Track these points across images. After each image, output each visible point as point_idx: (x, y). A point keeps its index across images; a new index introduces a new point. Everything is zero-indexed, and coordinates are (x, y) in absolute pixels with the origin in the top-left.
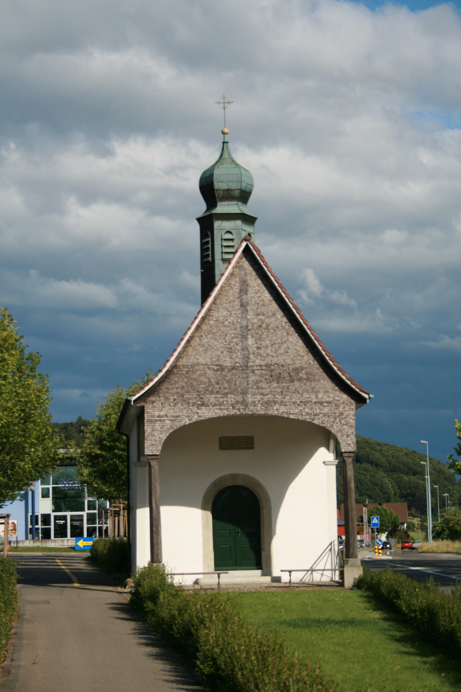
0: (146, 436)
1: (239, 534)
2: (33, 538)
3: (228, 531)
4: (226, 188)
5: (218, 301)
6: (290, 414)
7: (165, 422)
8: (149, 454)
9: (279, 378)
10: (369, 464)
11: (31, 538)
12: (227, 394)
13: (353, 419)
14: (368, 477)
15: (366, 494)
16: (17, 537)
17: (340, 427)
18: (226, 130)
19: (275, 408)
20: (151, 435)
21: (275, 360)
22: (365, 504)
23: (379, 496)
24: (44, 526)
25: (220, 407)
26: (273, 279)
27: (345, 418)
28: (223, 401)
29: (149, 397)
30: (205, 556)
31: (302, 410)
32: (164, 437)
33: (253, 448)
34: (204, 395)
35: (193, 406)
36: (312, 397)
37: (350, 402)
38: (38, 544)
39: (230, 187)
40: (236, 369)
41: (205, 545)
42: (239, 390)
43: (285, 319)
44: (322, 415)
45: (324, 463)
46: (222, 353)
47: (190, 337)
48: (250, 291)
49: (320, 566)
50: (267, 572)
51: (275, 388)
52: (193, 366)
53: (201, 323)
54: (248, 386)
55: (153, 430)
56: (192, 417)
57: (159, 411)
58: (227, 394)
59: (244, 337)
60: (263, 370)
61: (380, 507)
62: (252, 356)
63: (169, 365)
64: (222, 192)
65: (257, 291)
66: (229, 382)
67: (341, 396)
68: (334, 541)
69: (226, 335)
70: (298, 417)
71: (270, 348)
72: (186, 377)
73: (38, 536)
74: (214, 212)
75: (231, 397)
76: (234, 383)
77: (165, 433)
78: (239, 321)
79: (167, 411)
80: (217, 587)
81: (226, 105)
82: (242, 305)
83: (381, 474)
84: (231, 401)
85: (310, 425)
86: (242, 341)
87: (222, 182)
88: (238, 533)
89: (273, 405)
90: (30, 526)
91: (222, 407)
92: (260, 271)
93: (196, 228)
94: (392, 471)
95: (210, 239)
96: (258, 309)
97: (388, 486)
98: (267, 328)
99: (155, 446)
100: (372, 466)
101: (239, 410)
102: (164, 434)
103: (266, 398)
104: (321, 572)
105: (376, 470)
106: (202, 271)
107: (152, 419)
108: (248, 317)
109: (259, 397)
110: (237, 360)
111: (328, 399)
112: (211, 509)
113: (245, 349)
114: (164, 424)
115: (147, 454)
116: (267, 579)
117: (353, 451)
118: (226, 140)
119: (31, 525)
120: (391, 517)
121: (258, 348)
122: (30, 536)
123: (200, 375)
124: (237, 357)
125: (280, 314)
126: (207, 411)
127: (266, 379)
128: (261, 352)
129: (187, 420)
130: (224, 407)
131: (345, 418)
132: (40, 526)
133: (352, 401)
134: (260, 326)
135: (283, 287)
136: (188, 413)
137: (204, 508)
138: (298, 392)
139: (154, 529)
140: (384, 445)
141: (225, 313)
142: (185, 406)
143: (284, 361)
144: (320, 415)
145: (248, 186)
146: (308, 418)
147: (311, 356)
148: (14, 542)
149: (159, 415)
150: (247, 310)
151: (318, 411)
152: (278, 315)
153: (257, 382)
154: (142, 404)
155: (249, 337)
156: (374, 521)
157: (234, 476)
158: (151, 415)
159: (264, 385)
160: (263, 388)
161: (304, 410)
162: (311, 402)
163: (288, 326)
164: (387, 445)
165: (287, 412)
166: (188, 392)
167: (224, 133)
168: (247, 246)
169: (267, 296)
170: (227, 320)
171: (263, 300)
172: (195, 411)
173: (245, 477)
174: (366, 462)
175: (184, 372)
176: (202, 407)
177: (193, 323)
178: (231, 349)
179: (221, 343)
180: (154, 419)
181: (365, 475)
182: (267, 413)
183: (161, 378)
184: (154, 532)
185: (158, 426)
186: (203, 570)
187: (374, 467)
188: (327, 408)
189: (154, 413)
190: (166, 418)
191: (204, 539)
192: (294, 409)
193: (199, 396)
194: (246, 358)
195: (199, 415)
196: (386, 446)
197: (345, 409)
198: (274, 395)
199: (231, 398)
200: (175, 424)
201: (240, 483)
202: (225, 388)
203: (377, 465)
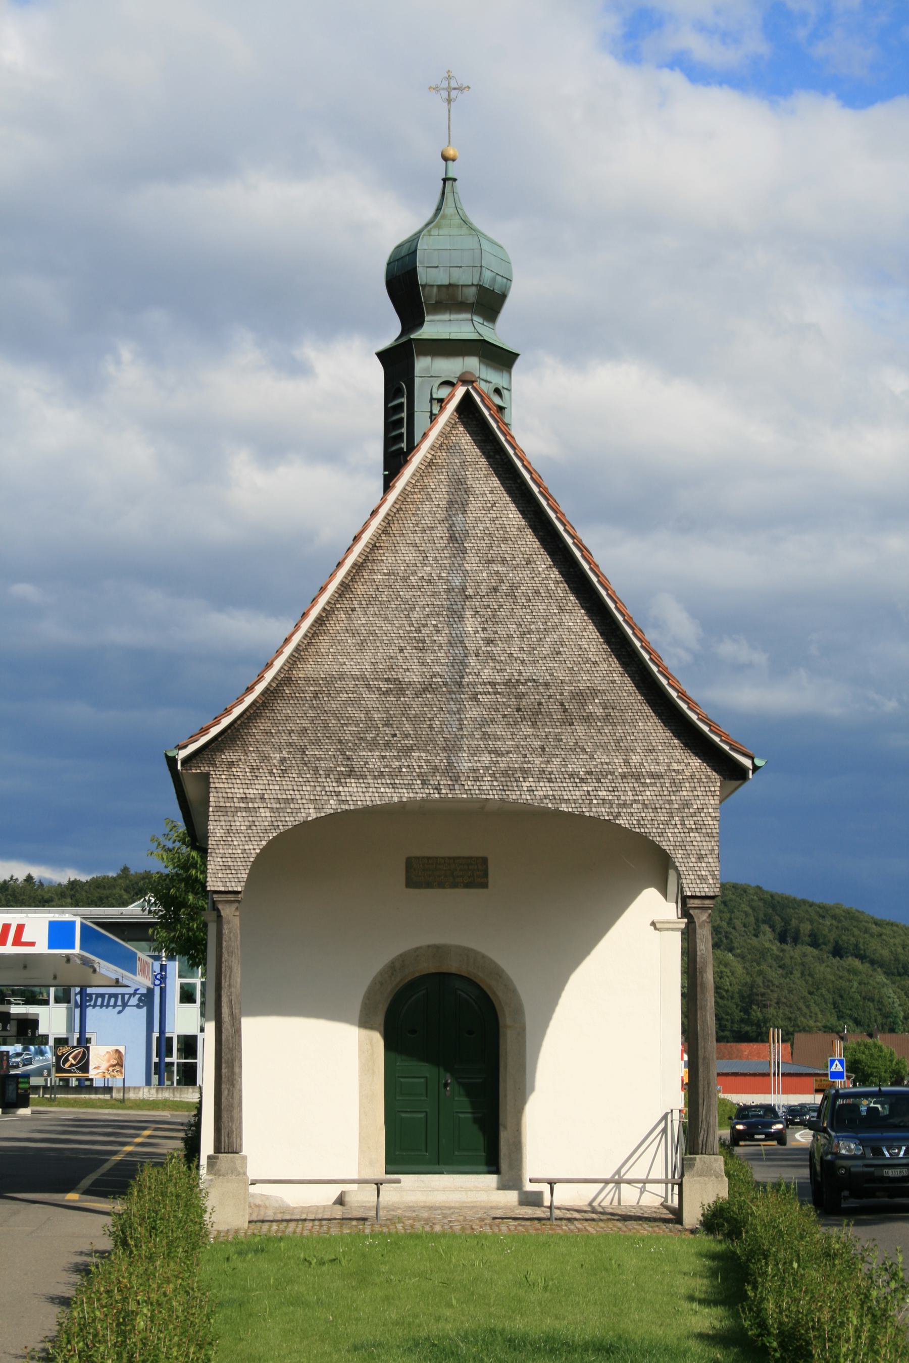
0: (210, 846)
1: (448, 1088)
2: (161, 1083)
3: (423, 1080)
4: (446, 282)
5: (395, 527)
6: (562, 800)
7: (258, 814)
8: (217, 889)
9: (536, 716)
10: (857, 960)
11: (157, 1083)
12: (410, 749)
13: (713, 818)
14: (855, 984)
15: (850, 1016)
16: (124, 1079)
17: (682, 835)
18: (451, 152)
19: (525, 785)
20: (222, 843)
21: (528, 671)
22: (842, 1034)
23: (876, 1021)
24: (185, 1058)
25: (392, 782)
26: (527, 476)
27: (694, 815)
28: (400, 767)
29: (222, 751)
30: (363, 1139)
31: (591, 793)
32: (255, 848)
33: (485, 885)
34: (354, 751)
35: (327, 776)
36: (616, 761)
37: (708, 777)
38: (166, 1095)
39: (453, 281)
40: (433, 691)
41: (364, 1113)
42: (440, 740)
43: (555, 574)
44: (640, 806)
45: (653, 924)
46: (401, 651)
47: (324, 609)
48: (474, 505)
49: (637, 1172)
50: (512, 1182)
51: (526, 737)
52: (330, 680)
53: (352, 580)
54: (461, 733)
55: (229, 831)
56: (323, 802)
57: (245, 786)
58: (410, 749)
59: (455, 615)
60: (499, 693)
61: (869, 1041)
62: (472, 660)
63: (269, 675)
64: (435, 289)
65: (489, 505)
66: (415, 721)
67: (686, 761)
68: (672, 1111)
69: (413, 609)
70: (579, 810)
71: (517, 641)
72: (312, 707)
73: (171, 1079)
74: (412, 336)
75: (420, 758)
76: (428, 723)
77: (258, 839)
78: (443, 575)
79: (263, 787)
80: (373, 1213)
81: (454, 94)
82: (452, 538)
83: (881, 978)
84: (420, 767)
85: (610, 827)
86: (449, 625)
87: (437, 267)
88: (446, 1085)
89: (521, 779)
90: (155, 1059)
91: (397, 781)
92: (497, 457)
93: (376, 375)
94: (899, 975)
95: (404, 400)
96: (490, 547)
97: (893, 1003)
98: (511, 594)
99: (233, 872)
100: (862, 963)
101: (438, 789)
102: (254, 843)
103: (503, 762)
104: (640, 1185)
105: (870, 972)
106: (387, 473)
107: (228, 805)
108: (466, 565)
109: (486, 759)
110: (437, 669)
111: (654, 768)
112: (382, 1028)
113: (457, 641)
114: (254, 819)
115: (213, 889)
116: (511, 1197)
117: (712, 894)
118: (450, 175)
119: (157, 1057)
120: (891, 1061)
121: (489, 642)
122: (155, 1079)
123: (345, 704)
124: (436, 661)
125: (543, 562)
126: (360, 789)
127: (504, 716)
128: (496, 650)
129: (312, 811)
130: (401, 782)
131: (694, 815)
132: (174, 1059)
133: (715, 775)
134: (495, 589)
135: (551, 496)
136: (315, 793)
137: (365, 1023)
138: (583, 750)
139: (224, 1071)
140: (888, 924)
141: (411, 556)
142: (308, 776)
143: (552, 675)
144: (635, 806)
145: (499, 278)
146: (604, 813)
147: (615, 663)
148: (118, 1090)
149: (243, 796)
150: (464, 551)
151: (630, 797)
152: (538, 563)
153: (483, 723)
154: (205, 769)
155: (468, 613)
156: (834, 1066)
157: (438, 951)
158: (225, 795)
159: (497, 729)
160: (496, 738)
161: (595, 793)
162: (612, 773)
163: (562, 590)
164: (892, 924)
165: (553, 795)
166: (316, 743)
167: (446, 159)
168: (467, 396)
169: (513, 516)
170: (414, 573)
171: (503, 527)
172: (332, 789)
173: (467, 953)
174: (852, 955)
175: (308, 696)
176: (348, 780)
177: (332, 575)
178: (424, 642)
179: (398, 628)
180: (232, 805)
181: (850, 981)
182: (505, 797)
183: (250, 706)
184: (224, 1079)
185: (240, 822)
186: (359, 1172)
187: (867, 965)
188: (651, 789)
189: (233, 791)
190: (261, 805)
191: (362, 1097)
192: (571, 789)
193: (343, 753)
194: (459, 665)
195: (340, 798)
196: (890, 927)
197: (695, 793)
198: (525, 756)
199: (419, 760)
200: (283, 819)
201: (453, 966)
202: (407, 736)
203: (872, 962)
